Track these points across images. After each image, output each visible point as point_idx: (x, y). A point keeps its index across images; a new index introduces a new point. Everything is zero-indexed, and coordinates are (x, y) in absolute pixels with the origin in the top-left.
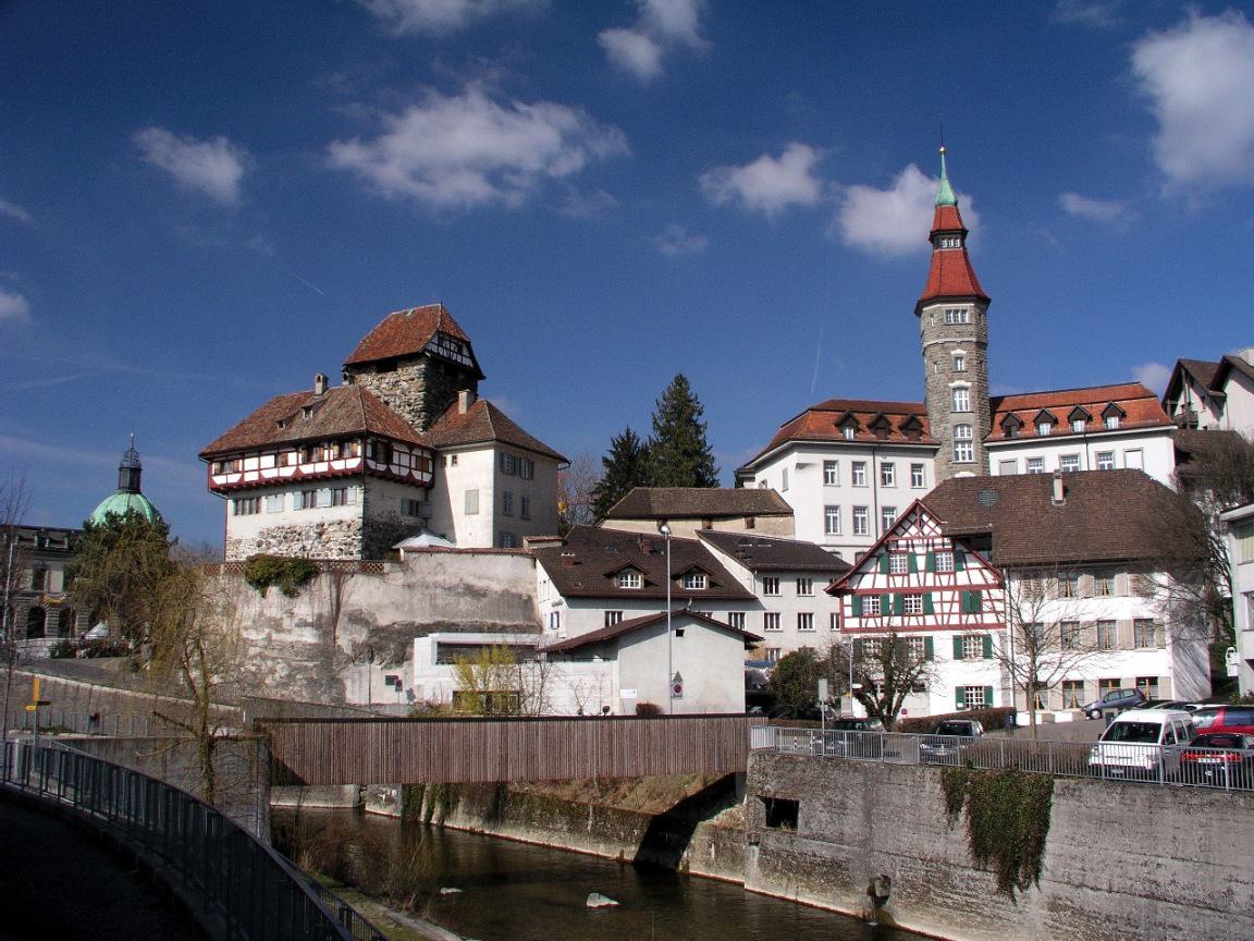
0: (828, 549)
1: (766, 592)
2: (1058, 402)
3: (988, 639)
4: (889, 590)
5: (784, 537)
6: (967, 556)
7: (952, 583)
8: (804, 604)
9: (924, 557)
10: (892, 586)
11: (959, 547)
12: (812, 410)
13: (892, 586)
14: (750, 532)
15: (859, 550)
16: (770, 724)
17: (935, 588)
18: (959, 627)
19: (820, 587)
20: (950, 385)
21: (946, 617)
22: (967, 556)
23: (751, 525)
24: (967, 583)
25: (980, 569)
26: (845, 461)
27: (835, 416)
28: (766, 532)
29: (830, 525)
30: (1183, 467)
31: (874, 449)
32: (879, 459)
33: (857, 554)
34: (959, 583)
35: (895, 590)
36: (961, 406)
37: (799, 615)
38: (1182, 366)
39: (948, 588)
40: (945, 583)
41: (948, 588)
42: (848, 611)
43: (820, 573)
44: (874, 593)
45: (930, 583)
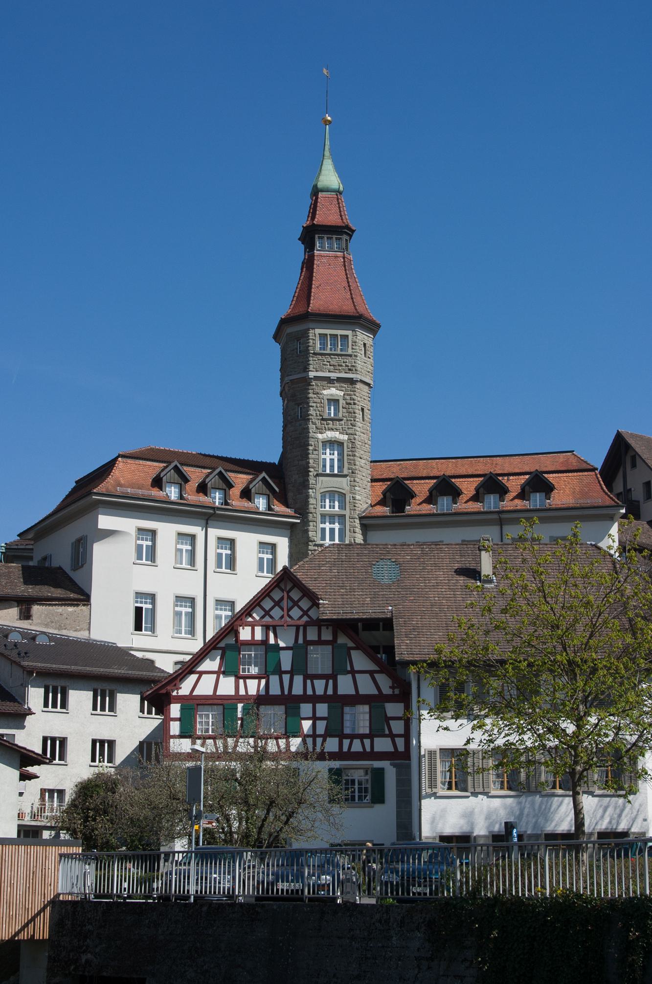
0: (139, 655)
1: (46, 705)
2: (462, 471)
3: (378, 776)
4: (237, 698)
5: (72, 634)
6: (353, 652)
7: (330, 692)
8: (102, 727)
9: (290, 653)
10: (242, 692)
11: (342, 640)
12: (123, 456)
13: (242, 692)
14: (25, 624)
15: (180, 658)
16: (85, 858)
17: (304, 698)
18: (333, 756)
19: (129, 702)
20: (320, 436)
21: (319, 741)
22: (353, 652)
23: (26, 615)
24: (352, 692)
25: (371, 673)
26: (167, 532)
27: (154, 468)
28: (47, 625)
29: (140, 620)
30: (543, 836)
31: (208, 517)
32: (214, 533)
33: (176, 663)
34: (341, 692)
35: (246, 698)
36: (332, 466)
37: (94, 742)
38: (628, 447)
39: (323, 699)
40: (320, 691)
41: (323, 699)
42: (175, 728)
43: (128, 683)
44: (213, 701)
45: (298, 690)
